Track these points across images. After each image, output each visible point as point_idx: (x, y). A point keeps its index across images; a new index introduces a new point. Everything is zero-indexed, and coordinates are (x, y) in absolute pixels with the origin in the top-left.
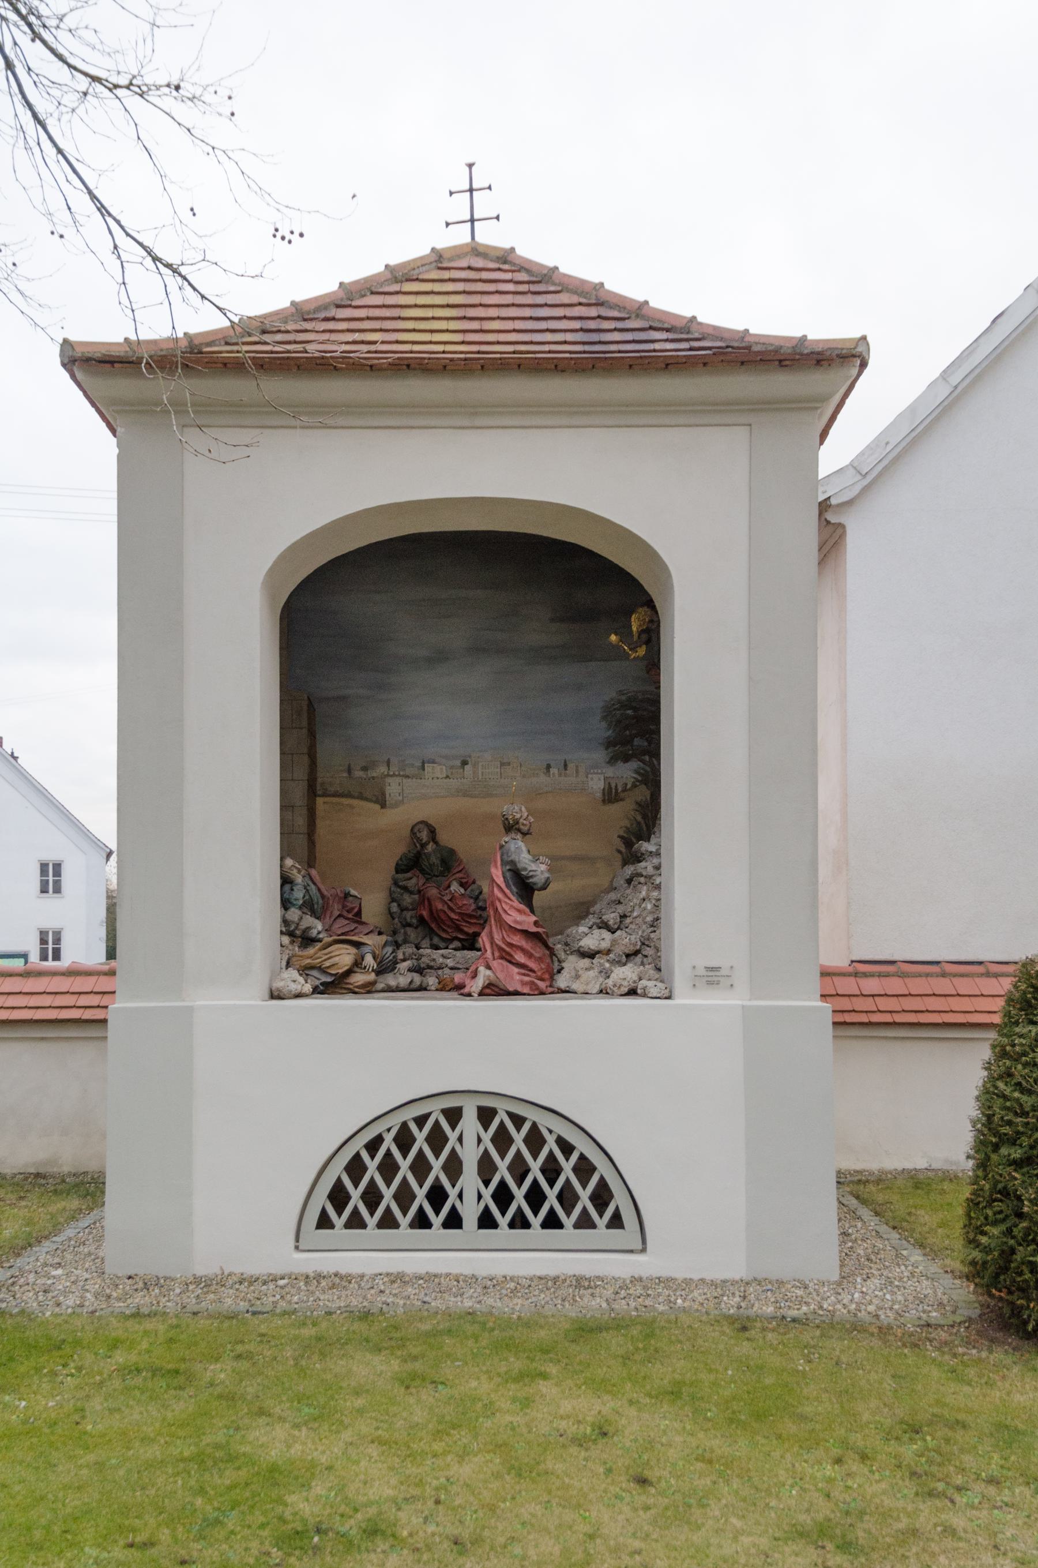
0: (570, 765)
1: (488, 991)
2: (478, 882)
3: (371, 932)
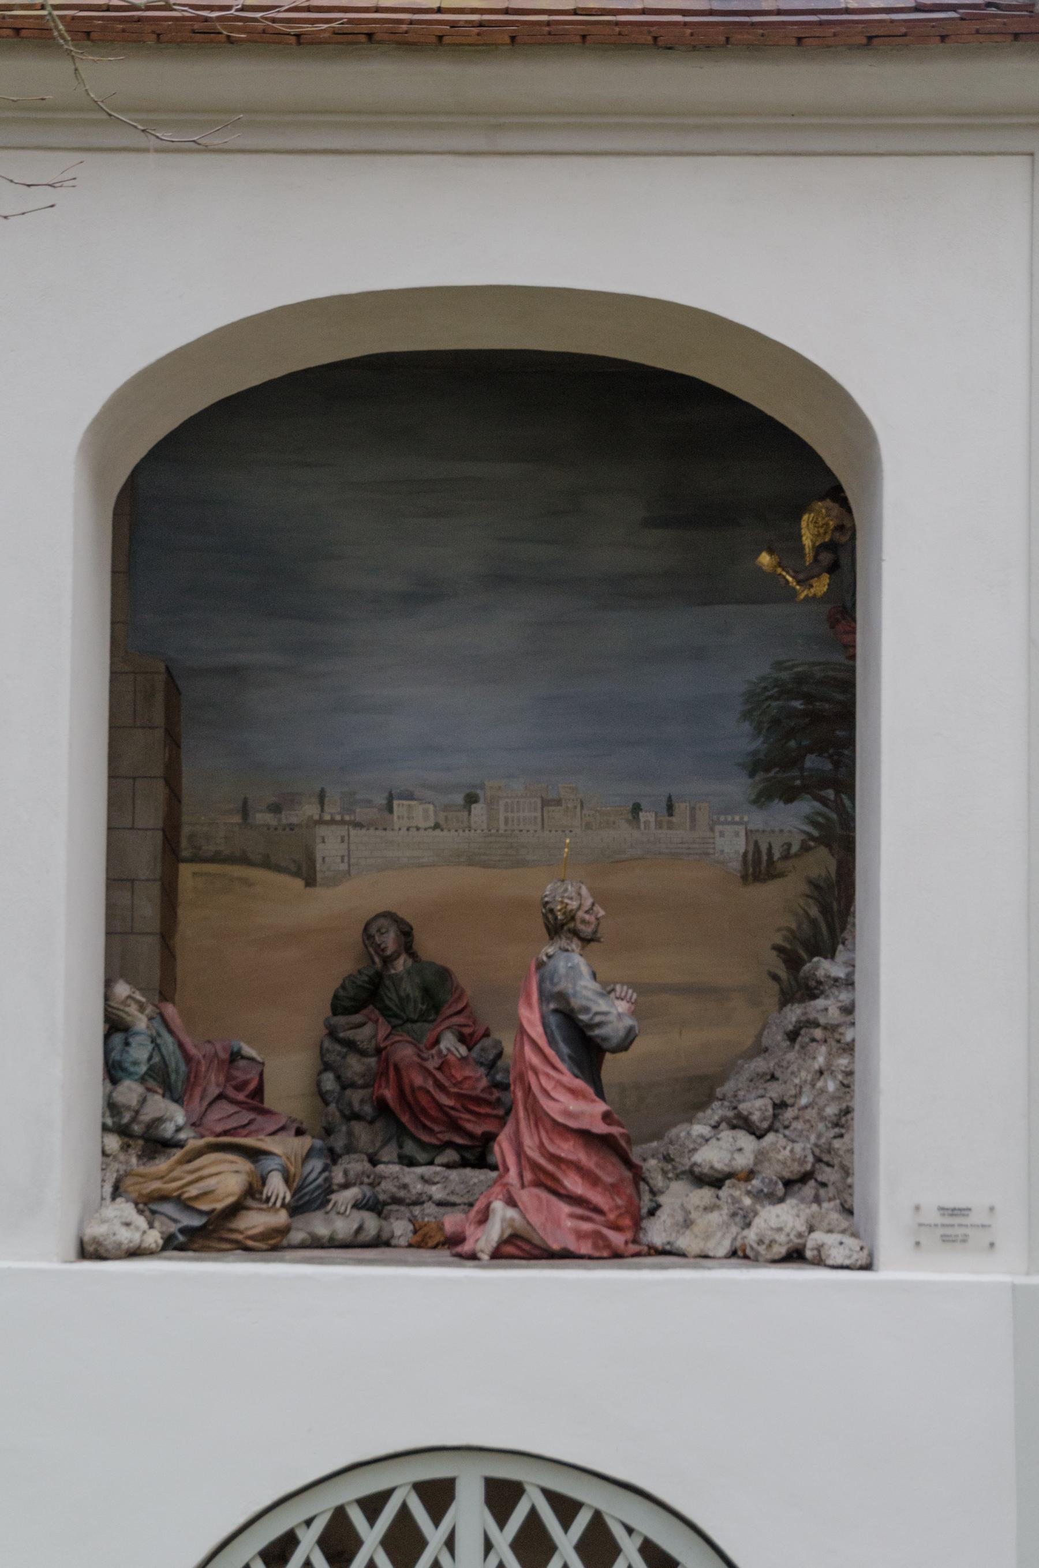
0: (681, 808)
1: (509, 1249)
3: (283, 1129)
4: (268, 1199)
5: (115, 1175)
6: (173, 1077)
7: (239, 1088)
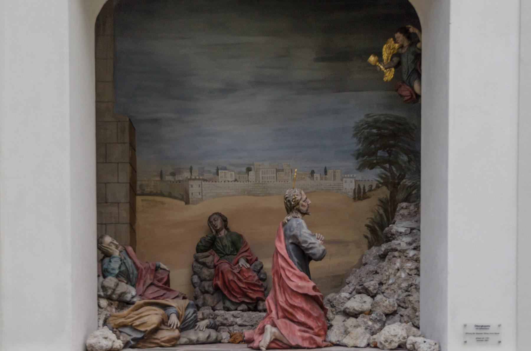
0: (330, 172)
1: (273, 345)
2: (260, 260)
3: (177, 297)
4: (170, 325)
5: (104, 316)
6: (131, 276)
7: (159, 281)
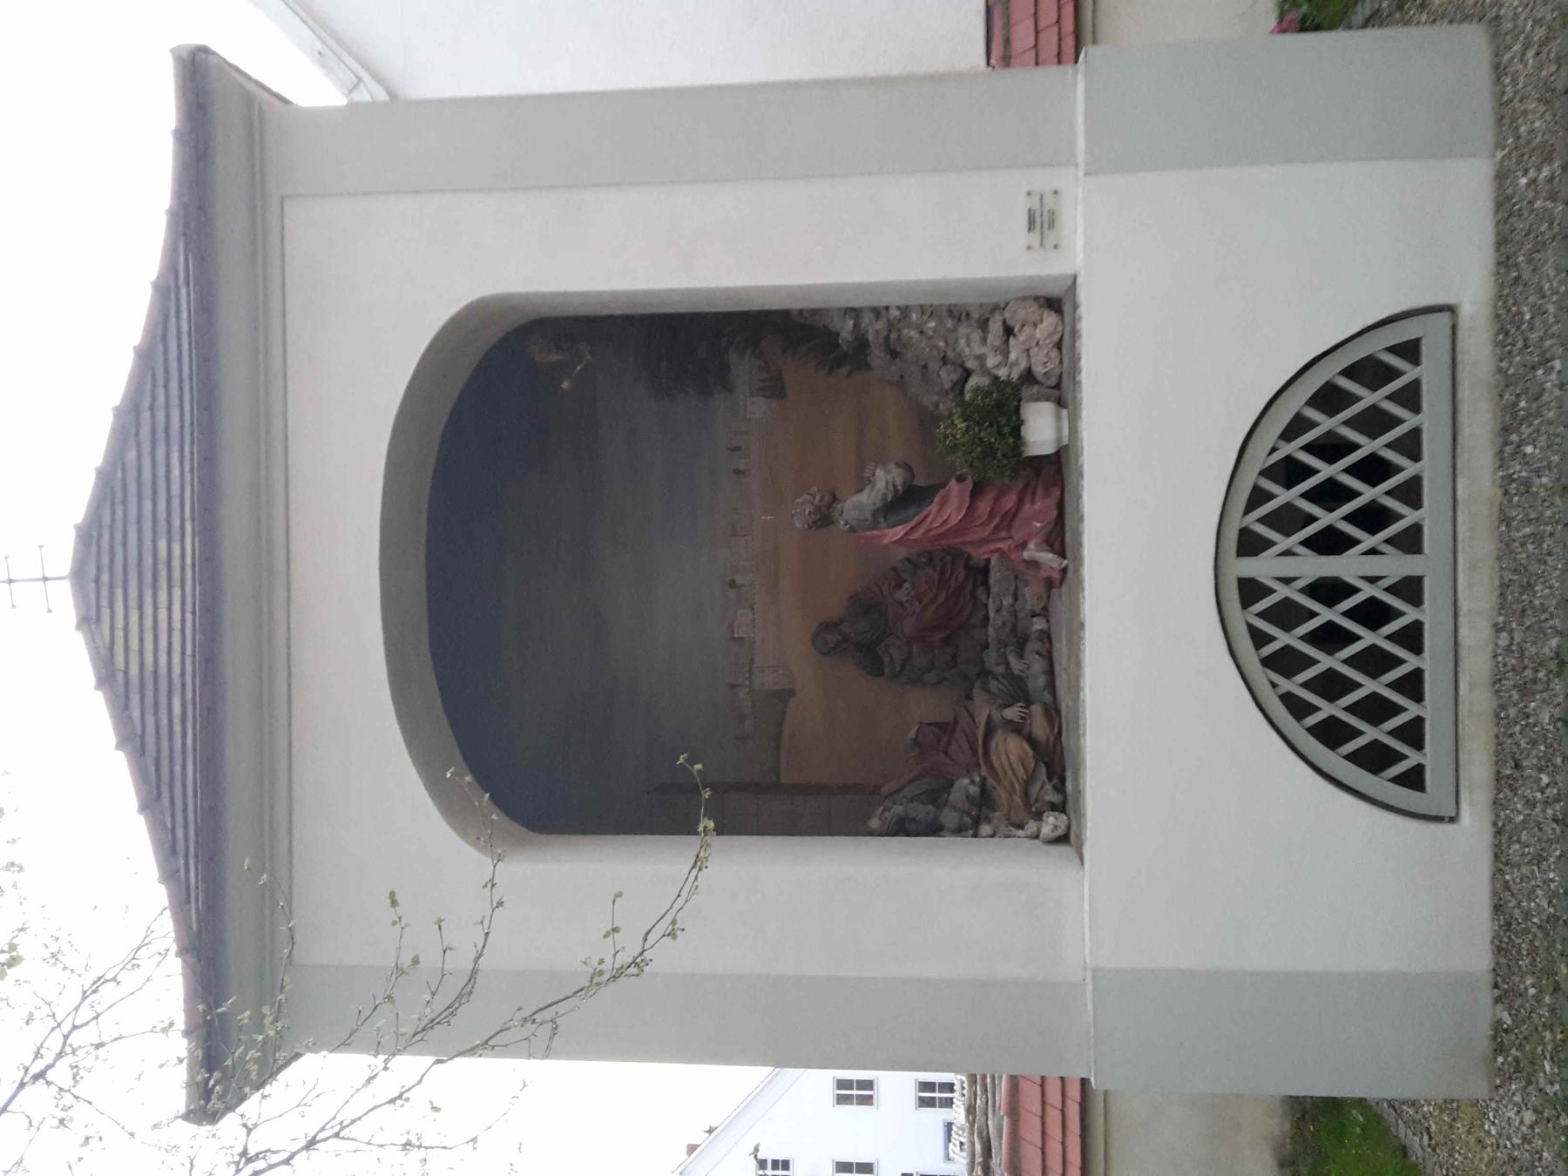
7: (939, 741)
